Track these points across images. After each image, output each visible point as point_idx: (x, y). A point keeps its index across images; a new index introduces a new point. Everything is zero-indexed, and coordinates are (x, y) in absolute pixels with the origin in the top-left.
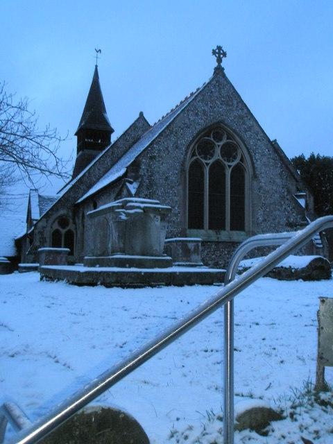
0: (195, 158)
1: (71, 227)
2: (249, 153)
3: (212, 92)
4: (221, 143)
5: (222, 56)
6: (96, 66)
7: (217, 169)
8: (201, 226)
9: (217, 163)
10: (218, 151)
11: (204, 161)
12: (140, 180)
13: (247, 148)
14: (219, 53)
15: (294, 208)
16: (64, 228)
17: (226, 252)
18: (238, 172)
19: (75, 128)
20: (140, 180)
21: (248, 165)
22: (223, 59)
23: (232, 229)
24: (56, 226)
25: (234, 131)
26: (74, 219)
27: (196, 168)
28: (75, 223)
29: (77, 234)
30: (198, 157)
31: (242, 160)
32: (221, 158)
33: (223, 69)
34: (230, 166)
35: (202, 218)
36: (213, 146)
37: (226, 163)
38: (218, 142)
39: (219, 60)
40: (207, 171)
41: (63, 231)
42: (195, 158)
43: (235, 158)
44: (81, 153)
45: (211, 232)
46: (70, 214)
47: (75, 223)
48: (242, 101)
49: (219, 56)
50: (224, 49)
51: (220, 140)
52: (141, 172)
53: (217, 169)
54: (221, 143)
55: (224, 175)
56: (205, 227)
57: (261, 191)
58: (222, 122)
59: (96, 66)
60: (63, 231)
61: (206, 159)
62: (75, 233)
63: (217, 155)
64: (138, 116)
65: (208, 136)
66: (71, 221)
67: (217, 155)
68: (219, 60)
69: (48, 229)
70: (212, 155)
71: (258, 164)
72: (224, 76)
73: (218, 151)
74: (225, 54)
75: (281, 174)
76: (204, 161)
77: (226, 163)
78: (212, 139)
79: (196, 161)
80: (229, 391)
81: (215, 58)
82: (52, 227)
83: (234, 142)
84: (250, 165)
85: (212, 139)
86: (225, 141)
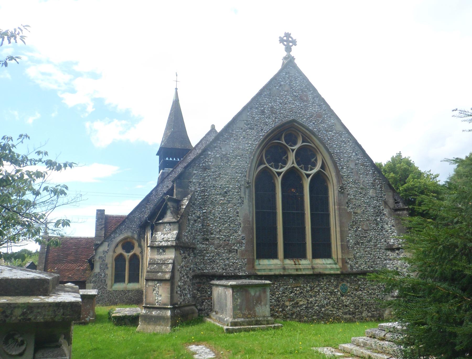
0: (262, 166)
1: (136, 250)
2: (331, 157)
3: (281, 85)
4: (296, 147)
5: (291, 44)
6: (176, 89)
8: (274, 256)
9: (292, 171)
10: (292, 157)
11: (274, 170)
12: (190, 196)
13: (330, 154)
14: (287, 41)
15: (393, 226)
16: (128, 251)
17: (309, 288)
20: (190, 196)
22: (293, 48)
23: (315, 256)
24: (120, 250)
25: (311, 131)
28: (140, 246)
29: (142, 259)
30: (267, 165)
31: (323, 167)
32: (296, 165)
33: (293, 58)
34: (308, 176)
35: (276, 245)
36: (285, 152)
37: (304, 172)
38: (291, 146)
39: (288, 49)
40: (279, 182)
41: (127, 255)
42: (262, 166)
43: (314, 165)
45: (289, 262)
46: (136, 236)
47: (140, 246)
48: (319, 96)
49: (288, 44)
50: (294, 36)
51: (295, 143)
54: (296, 147)
56: (308, 257)
57: (351, 205)
58: (294, 121)
59: (176, 89)
60: (127, 255)
61: (277, 168)
62: (140, 256)
63: (291, 162)
64: (209, 129)
65: (279, 139)
66: (136, 245)
67: (291, 162)
68: (288, 49)
69: (111, 253)
70: (285, 163)
72: (295, 66)
73: (292, 157)
74: (294, 42)
75: (373, 185)
76: (274, 170)
77: (304, 172)
78: (284, 143)
81: (282, 47)
82: (114, 252)
83: (313, 145)
84: (334, 174)
85: (284, 143)
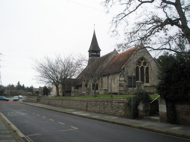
7: (142, 68)
9: (142, 66)
18: (147, 68)
19: (88, 49)
21: (149, 67)
23: (146, 83)
26: (98, 80)
27: (137, 68)
31: (148, 66)
44: (90, 58)
52: (125, 70)
53: (142, 68)
55: (144, 69)
63: (142, 65)
64: (114, 50)
67: (142, 65)
71: (152, 67)
79: (138, 66)
80: (140, 5)
86: (144, 61)
